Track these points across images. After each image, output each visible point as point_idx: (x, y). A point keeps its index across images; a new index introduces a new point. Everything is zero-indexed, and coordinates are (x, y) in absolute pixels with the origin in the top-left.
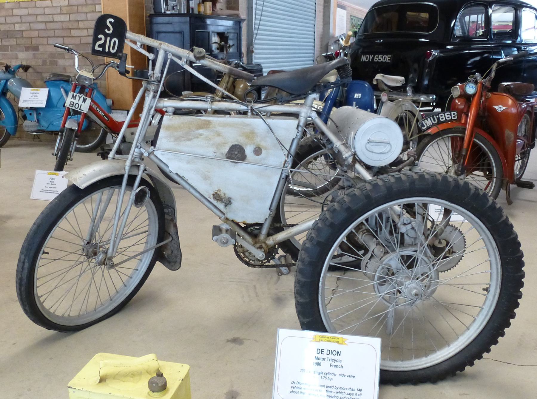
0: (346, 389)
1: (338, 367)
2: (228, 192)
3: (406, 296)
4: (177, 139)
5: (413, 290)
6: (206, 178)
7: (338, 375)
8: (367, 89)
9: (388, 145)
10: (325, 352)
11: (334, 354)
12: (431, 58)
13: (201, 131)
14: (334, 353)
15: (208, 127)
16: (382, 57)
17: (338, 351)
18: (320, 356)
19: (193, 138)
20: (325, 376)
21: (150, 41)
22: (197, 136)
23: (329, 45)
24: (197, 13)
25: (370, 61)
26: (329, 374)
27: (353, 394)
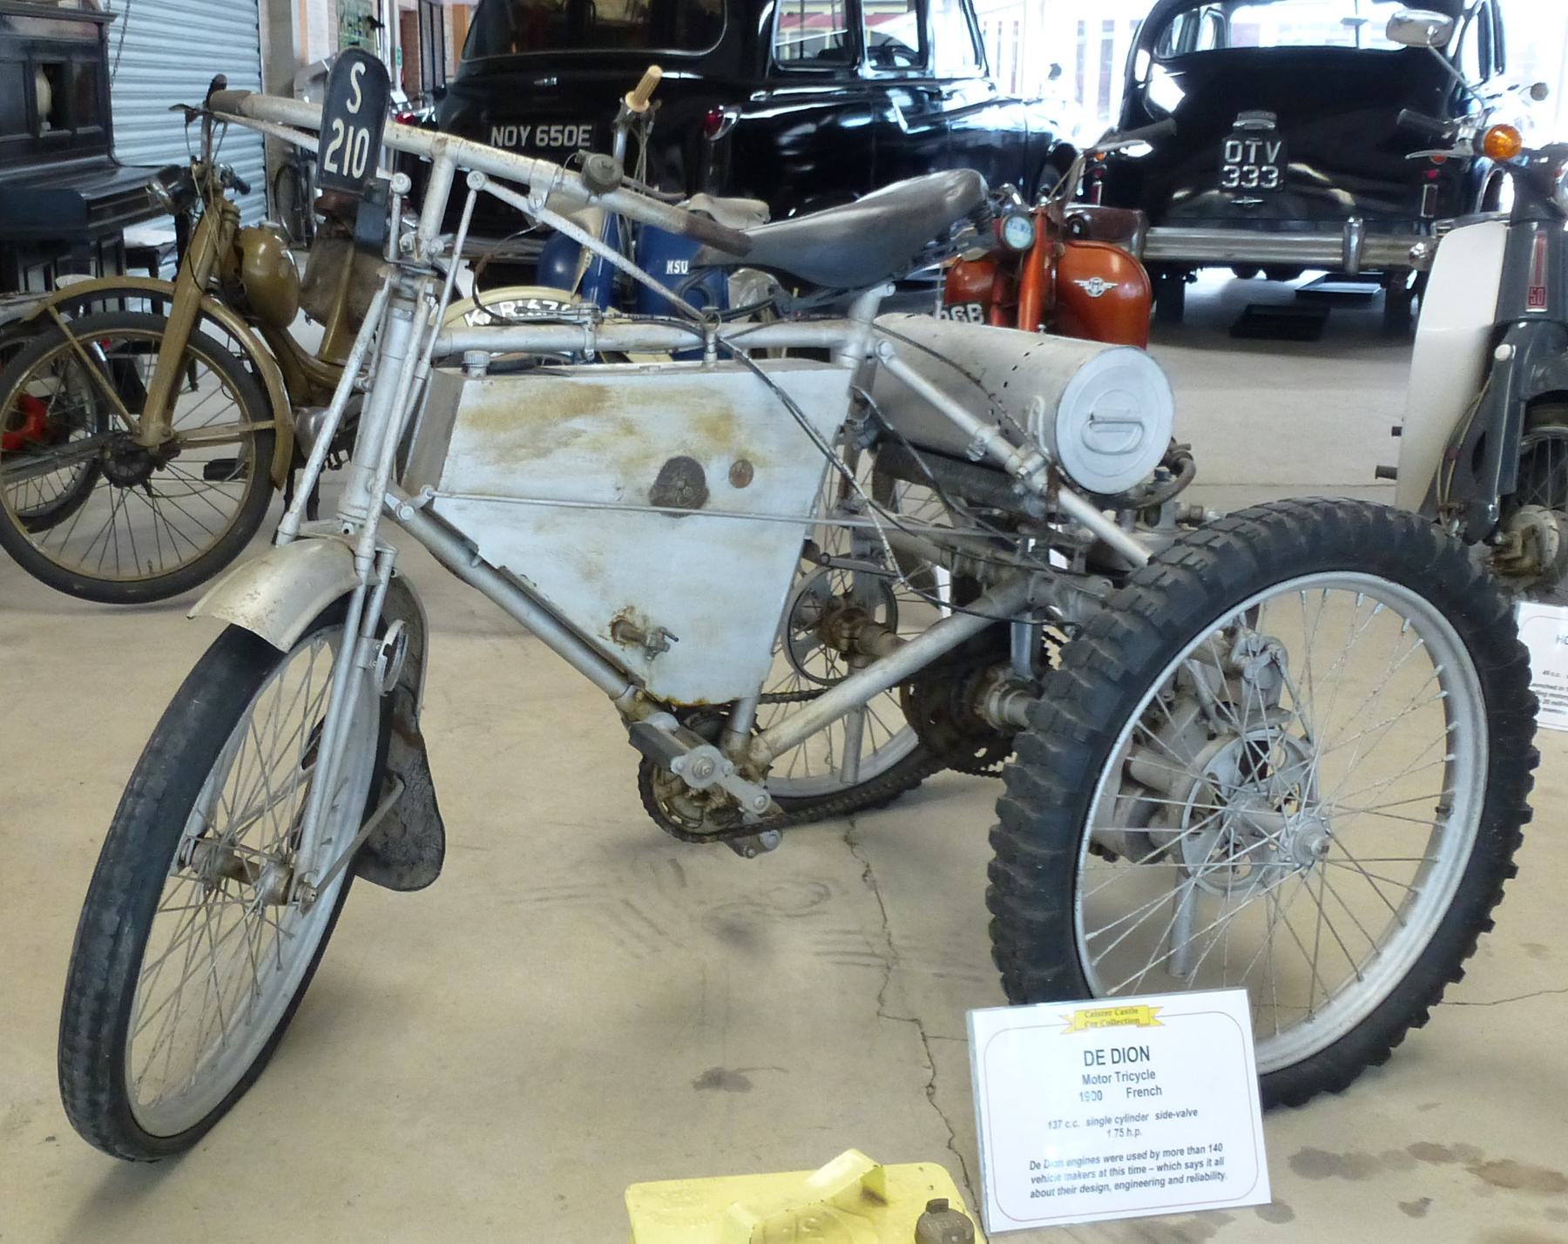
0: (1182, 1152)
1: (1149, 1092)
2: (656, 612)
3: (1288, 859)
4: (506, 454)
5: (1311, 837)
6: (590, 573)
7: (1152, 1117)
9: (1136, 429)
10: (1107, 1059)
11: (1133, 1058)
12: (719, 134)
13: (577, 423)
14: (1133, 1055)
15: (599, 409)
16: (562, 132)
17: (1141, 1049)
18: (1095, 1071)
19: (552, 446)
20: (1118, 1126)
21: (398, 130)
22: (564, 439)
23: (295, 88)
25: (523, 144)
26: (1127, 1118)
27: (1201, 1163)
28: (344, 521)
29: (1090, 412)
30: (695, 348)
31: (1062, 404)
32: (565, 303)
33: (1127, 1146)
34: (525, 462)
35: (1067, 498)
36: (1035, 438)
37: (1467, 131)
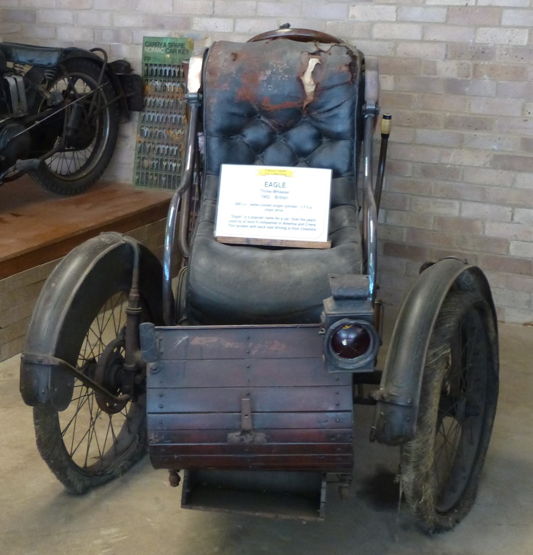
24: (367, 397)
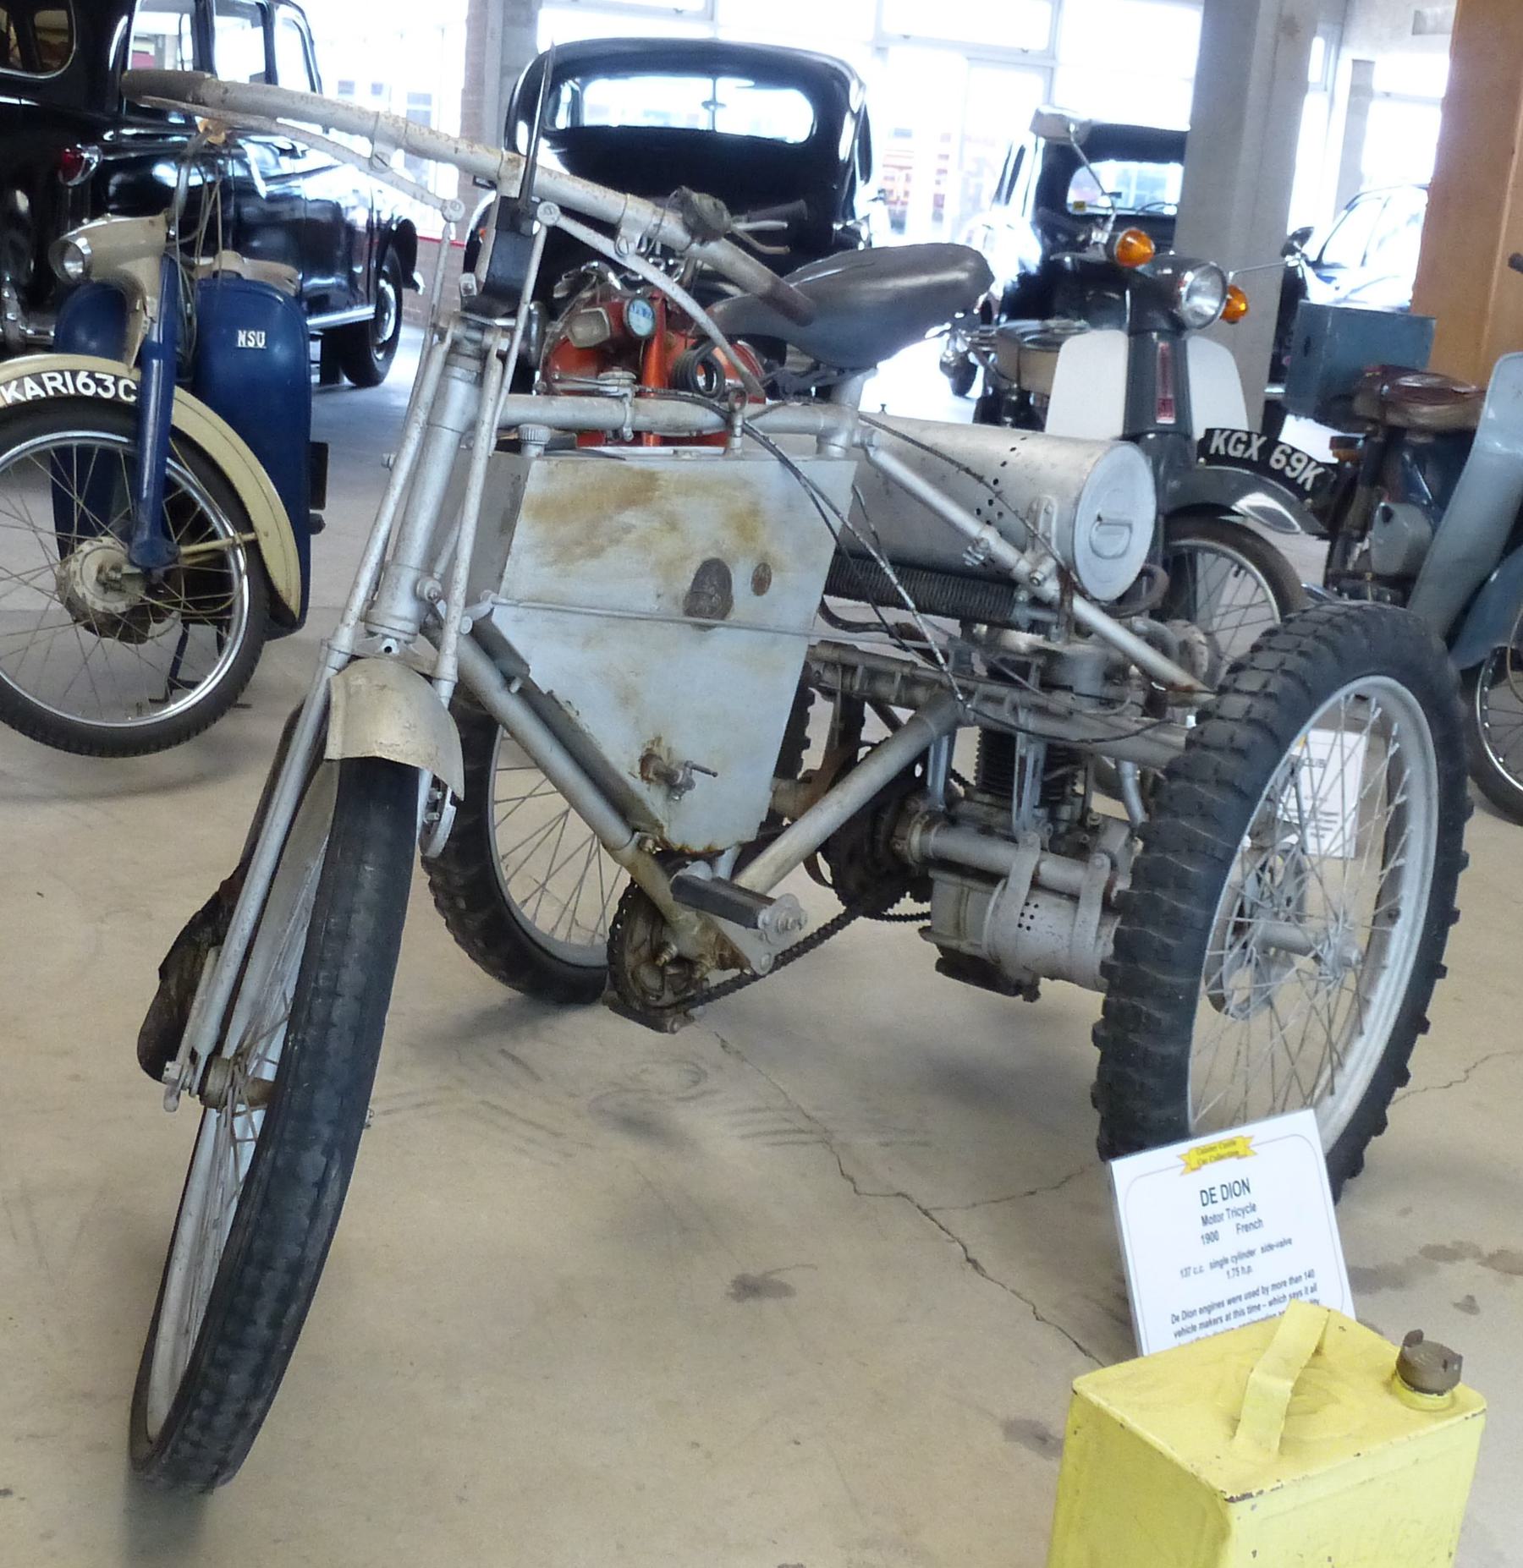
2: (684, 746)
6: (627, 698)
7: (1258, 1251)
8: (279, 309)
10: (1218, 1197)
12: (78, 180)
18: (1211, 1210)
20: (1234, 1266)
26: (1241, 1256)
27: (1221, 1319)
28: (386, 636)
29: (1097, 513)
30: (716, 431)
31: (1081, 504)
32: (122, 378)
33: (1242, 1285)
34: (582, 562)
35: (1080, 607)
36: (1048, 540)
37: (1100, 235)
